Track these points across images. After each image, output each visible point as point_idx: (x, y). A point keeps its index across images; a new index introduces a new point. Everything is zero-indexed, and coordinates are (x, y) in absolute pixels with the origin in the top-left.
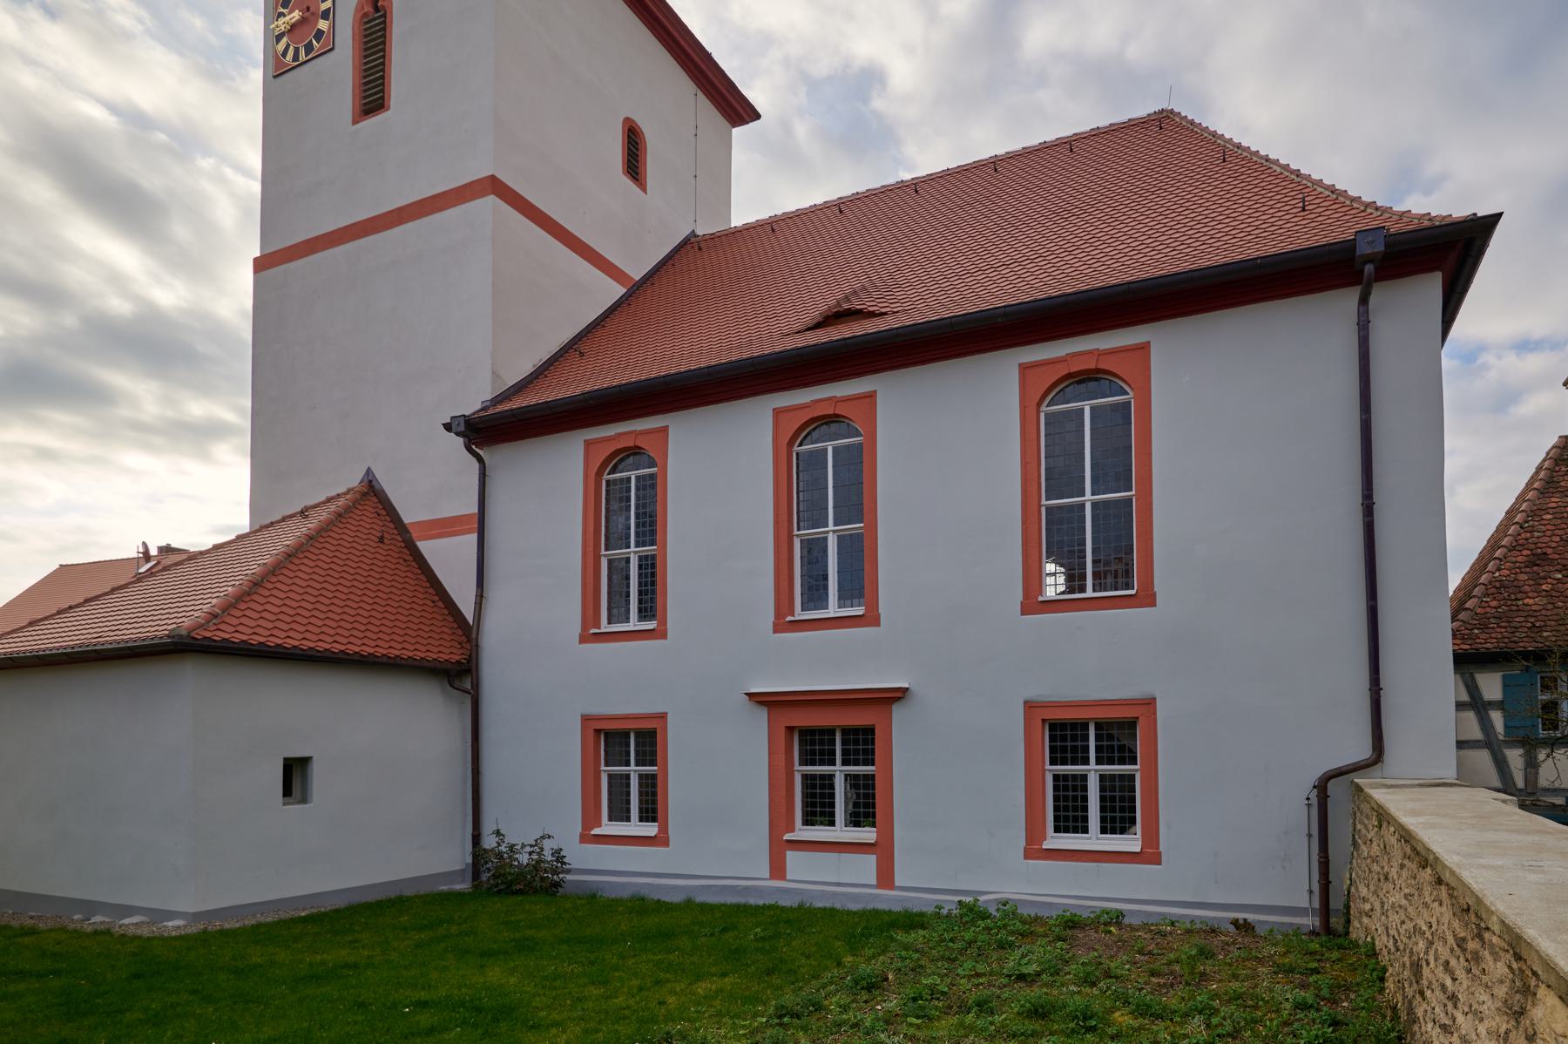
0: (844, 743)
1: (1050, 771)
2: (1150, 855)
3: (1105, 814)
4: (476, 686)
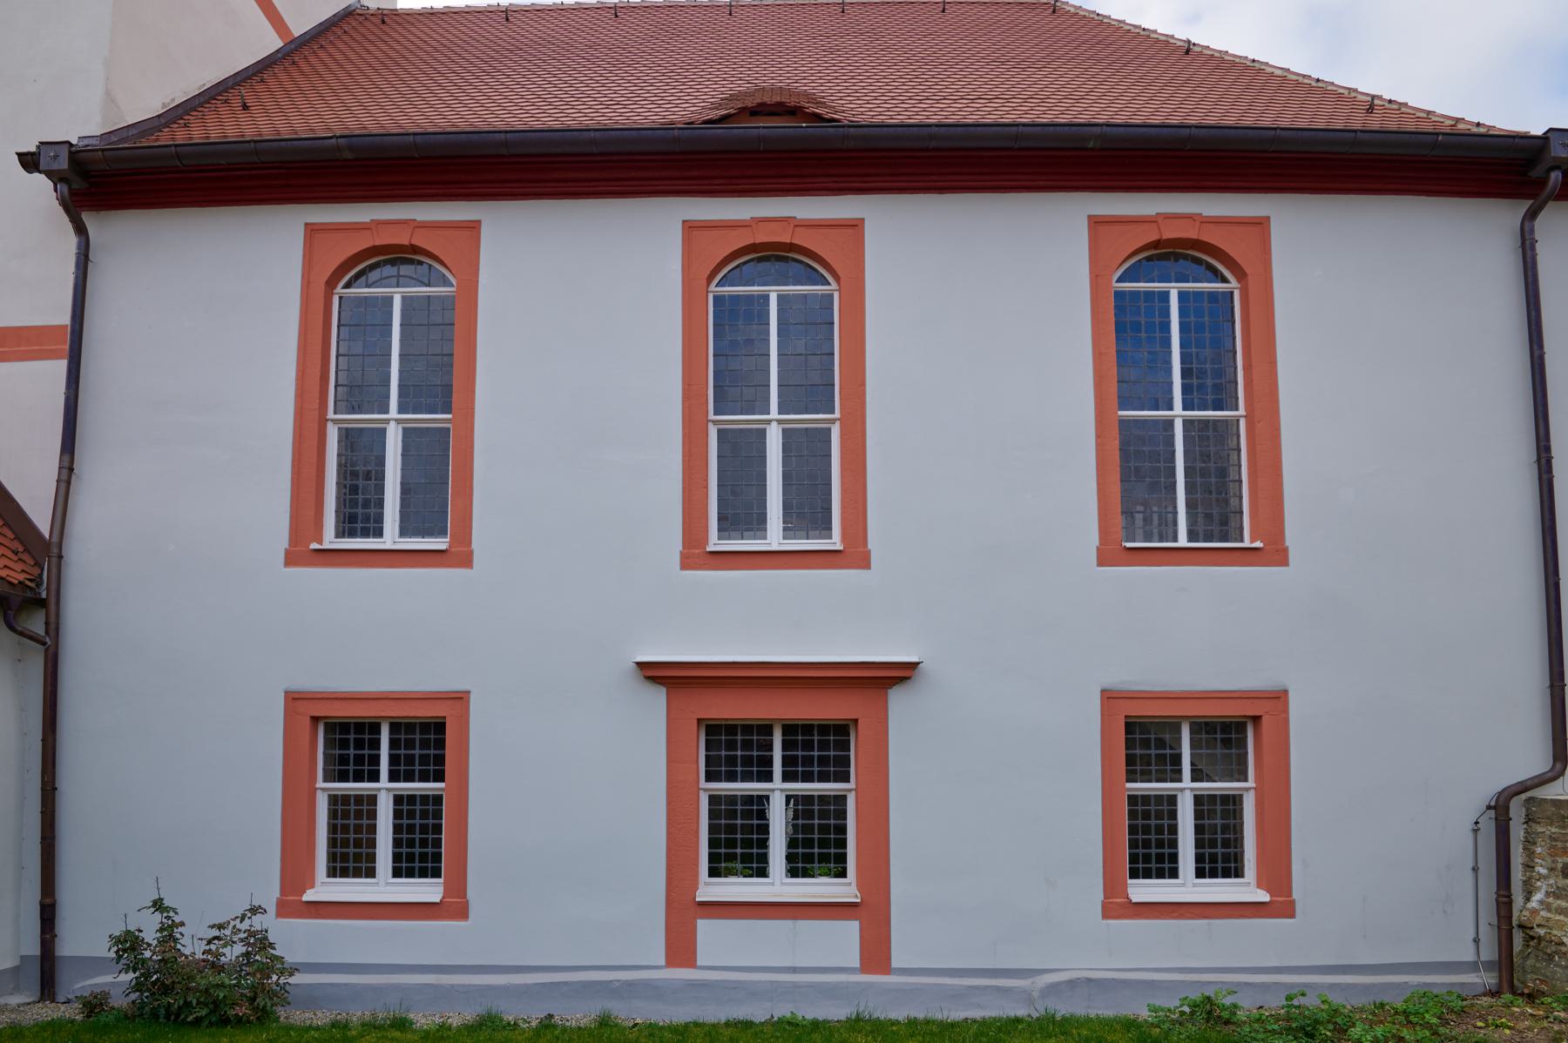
0: (786, 746)
1: (705, 790)
2: (454, 907)
3: (1202, 851)
4: (54, 628)
